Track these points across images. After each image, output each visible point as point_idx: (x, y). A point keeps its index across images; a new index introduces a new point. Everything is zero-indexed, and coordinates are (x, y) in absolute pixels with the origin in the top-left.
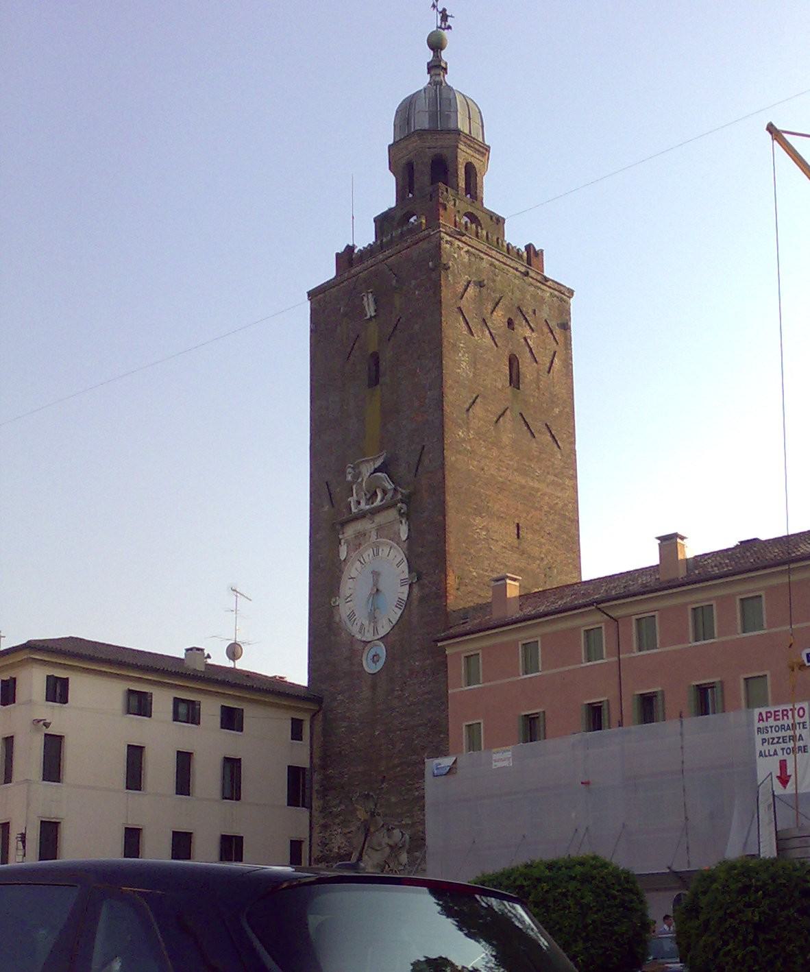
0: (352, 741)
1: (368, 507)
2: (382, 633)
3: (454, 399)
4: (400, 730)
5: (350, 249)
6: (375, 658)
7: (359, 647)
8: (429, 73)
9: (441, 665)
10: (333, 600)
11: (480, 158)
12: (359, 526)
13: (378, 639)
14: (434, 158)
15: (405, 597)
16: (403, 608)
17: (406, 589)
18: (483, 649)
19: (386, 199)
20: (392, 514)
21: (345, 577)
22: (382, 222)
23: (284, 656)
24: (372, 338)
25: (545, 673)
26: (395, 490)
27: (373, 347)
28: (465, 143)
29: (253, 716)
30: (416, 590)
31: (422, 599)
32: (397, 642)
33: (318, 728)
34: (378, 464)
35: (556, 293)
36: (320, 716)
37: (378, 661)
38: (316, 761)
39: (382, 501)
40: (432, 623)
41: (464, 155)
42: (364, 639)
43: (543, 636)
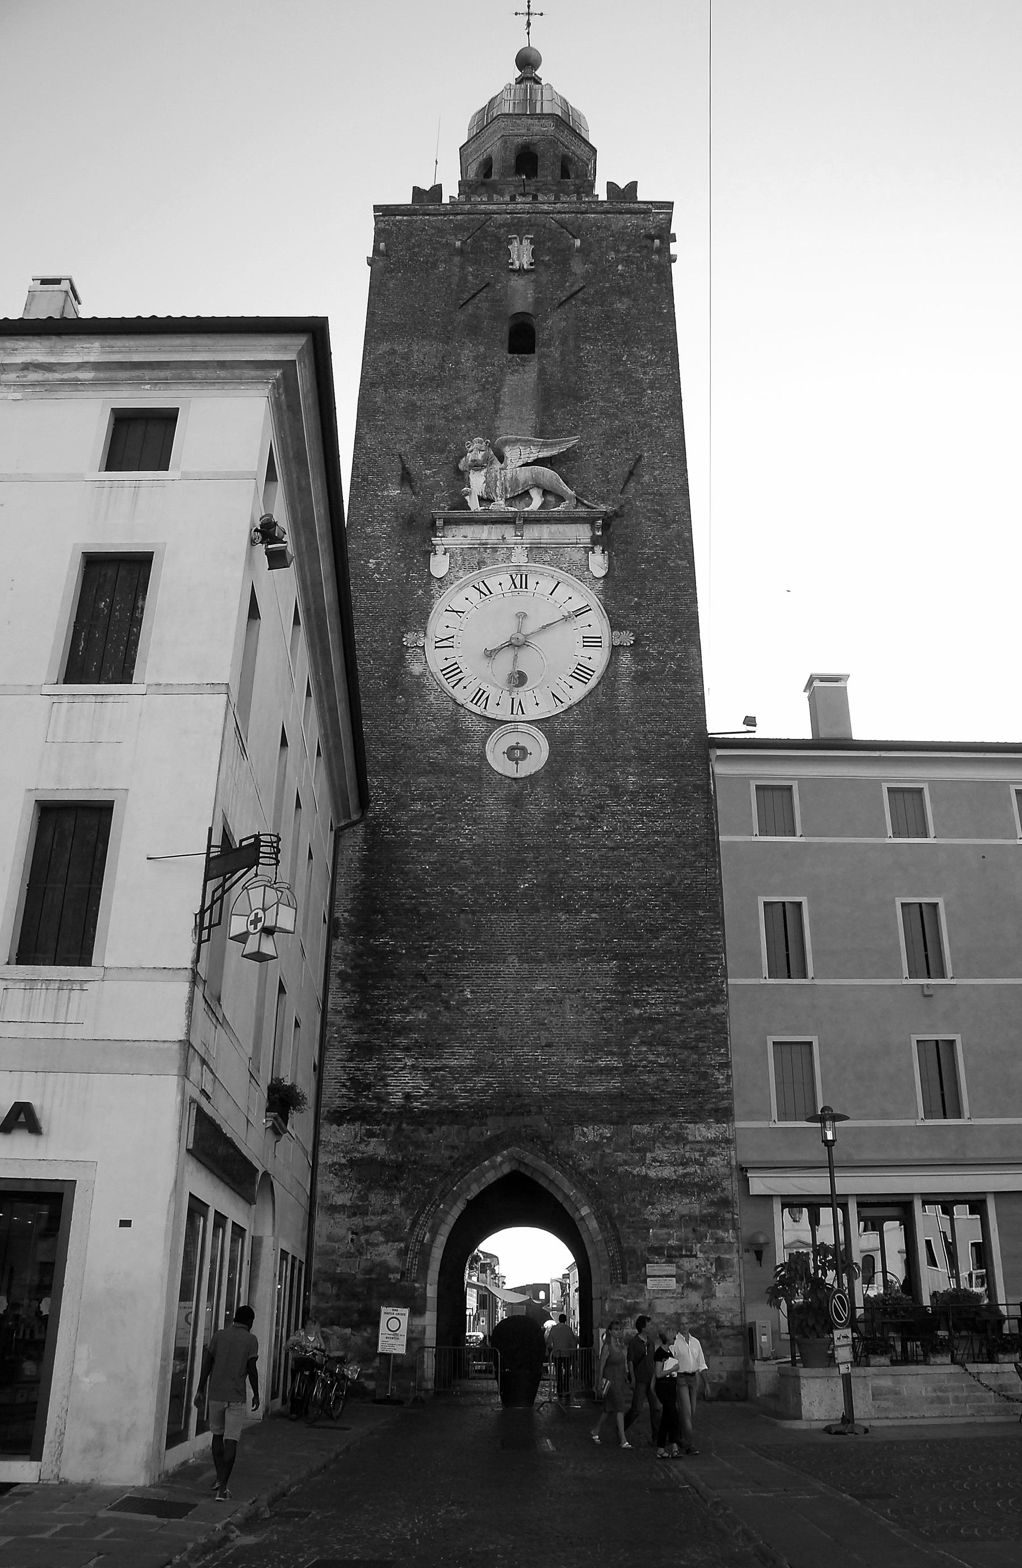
0: (452, 892)
4: (591, 889)
18: (801, 781)
20: (583, 533)
21: (439, 605)
24: (522, 296)
31: (641, 678)
34: (545, 453)
36: (360, 829)
37: (524, 758)
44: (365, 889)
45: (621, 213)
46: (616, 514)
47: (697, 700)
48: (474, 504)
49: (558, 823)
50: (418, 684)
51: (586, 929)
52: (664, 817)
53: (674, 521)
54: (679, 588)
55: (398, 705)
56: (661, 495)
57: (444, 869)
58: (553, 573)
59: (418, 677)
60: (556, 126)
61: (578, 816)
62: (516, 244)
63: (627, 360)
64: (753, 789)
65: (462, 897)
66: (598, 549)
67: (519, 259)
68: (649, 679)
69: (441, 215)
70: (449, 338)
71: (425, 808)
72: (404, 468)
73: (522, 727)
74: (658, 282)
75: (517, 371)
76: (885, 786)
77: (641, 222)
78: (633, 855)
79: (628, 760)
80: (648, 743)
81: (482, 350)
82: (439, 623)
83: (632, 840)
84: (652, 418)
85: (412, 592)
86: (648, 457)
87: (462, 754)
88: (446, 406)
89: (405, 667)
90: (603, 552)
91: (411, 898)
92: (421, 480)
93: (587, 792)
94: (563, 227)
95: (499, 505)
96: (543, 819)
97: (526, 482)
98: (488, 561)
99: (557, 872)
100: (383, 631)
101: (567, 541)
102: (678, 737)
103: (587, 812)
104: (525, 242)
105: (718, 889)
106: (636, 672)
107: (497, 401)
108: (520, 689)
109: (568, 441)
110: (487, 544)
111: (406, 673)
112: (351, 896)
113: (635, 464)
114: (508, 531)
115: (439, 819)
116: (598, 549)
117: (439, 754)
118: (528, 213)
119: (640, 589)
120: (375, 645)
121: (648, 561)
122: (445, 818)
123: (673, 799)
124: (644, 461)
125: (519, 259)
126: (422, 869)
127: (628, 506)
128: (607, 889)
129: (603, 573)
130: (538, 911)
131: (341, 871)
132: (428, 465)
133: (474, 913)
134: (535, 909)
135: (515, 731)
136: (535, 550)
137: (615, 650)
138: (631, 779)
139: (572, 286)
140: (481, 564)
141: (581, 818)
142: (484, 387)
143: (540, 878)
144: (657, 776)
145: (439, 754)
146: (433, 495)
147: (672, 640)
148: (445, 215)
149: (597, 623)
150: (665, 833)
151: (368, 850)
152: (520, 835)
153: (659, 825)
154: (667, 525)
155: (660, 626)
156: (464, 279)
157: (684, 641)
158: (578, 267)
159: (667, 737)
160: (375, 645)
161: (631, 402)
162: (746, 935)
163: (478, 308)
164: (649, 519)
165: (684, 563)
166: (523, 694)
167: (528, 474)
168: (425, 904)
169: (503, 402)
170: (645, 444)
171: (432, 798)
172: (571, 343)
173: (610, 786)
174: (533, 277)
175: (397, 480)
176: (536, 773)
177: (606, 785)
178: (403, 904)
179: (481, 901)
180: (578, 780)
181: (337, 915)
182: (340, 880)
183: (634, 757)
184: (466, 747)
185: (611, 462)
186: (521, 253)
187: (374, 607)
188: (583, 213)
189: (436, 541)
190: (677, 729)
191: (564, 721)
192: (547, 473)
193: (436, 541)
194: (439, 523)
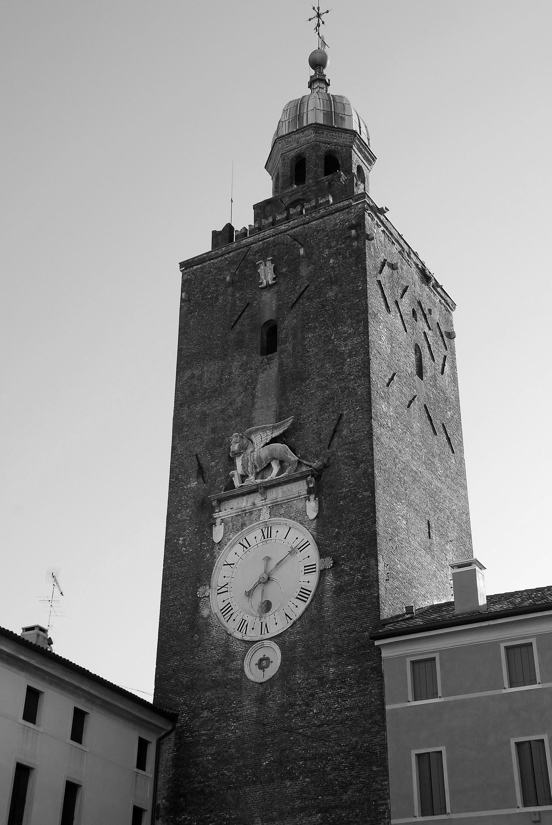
0: (223, 774)
1: (259, 481)
2: (274, 631)
3: (379, 370)
4: (305, 759)
5: (229, 228)
6: (264, 663)
7: (238, 648)
8: (310, 87)
9: (373, 672)
10: (201, 590)
11: (367, 165)
12: (244, 503)
13: (270, 639)
14: (319, 162)
15: (312, 587)
16: (309, 601)
17: (314, 578)
18: (441, 652)
19: (265, 190)
20: (301, 487)
21: (219, 562)
22: (261, 209)
23: (127, 656)
24: (268, 305)
25: (546, 685)
26: (299, 463)
27: (268, 315)
28: (358, 146)
29: (98, 723)
30: (329, 578)
31: (339, 590)
32: (301, 643)
33: (168, 754)
34: (276, 434)
35: (443, 301)
36: (172, 736)
37: (267, 666)
38: (161, 802)
39: (278, 474)
40: (351, 621)
41: (357, 159)
42: (246, 638)
43: (540, 637)
44: (174, 780)
45: (332, 214)
46: (325, 466)
47: (374, 600)
48: (237, 483)
49: (286, 712)
50: (206, 623)
51: (302, 791)
52: (351, 697)
53: (362, 462)
54: (364, 515)
55: (195, 641)
56: (354, 442)
57: (219, 758)
58: (285, 522)
59: (206, 619)
60: (316, 132)
61: (299, 704)
62: (262, 267)
63: (335, 338)
64: (408, 665)
65: (229, 777)
66: (312, 497)
67: (265, 278)
68: (344, 590)
69: (220, 256)
70: (225, 355)
71: (210, 714)
72: (199, 465)
73: (267, 643)
74: (356, 266)
75: (265, 369)
76: (502, 646)
77: (346, 217)
78: (331, 729)
79: (329, 656)
80: (342, 641)
81: (245, 358)
82: (220, 575)
83: (331, 717)
84: (349, 382)
85: (203, 556)
86: (347, 414)
87: (231, 670)
88: (223, 410)
89: (200, 612)
90: (315, 499)
91: (200, 782)
92: (208, 470)
93: (304, 686)
94: (295, 240)
95: (252, 480)
96: (277, 710)
97: (266, 458)
98: (247, 523)
99: (285, 750)
100: (186, 589)
101: (293, 496)
102: (362, 632)
103: (304, 700)
104: (268, 264)
105: (384, 747)
106: (335, 587)
107: (254, 396)
108: (268, 614)
109: (287, 421)
110: (246, 510)
111: (199, 617)
112: (167, 787)
113: (338, 422)
114: (257, 499)
115: (217, 721)
116: (312, 497)
117: (217, 673)
118: (273, 236)
119: (339, 521)
120: (182, 600)
121: (344, 498)
122: (221, 720)
123: (358, 681)
124: (344, 417)
125: (265, 278)
126: (208, 760)
127: (333, 458)
128: (316, 758)
129: (315, 514)
130: (273, 781)
131: (161, 769)
132: (213, 458)
133: (236, 788)
134: (271, 780)
135: (263, 647)
136: (275, 508)
137: (323, 573)
138: (332, 670)
139: (300, 288)
140: (243, 525)
141: (300, 706)
142: (246, 388)
143: (275, 756)
144: (348, 665)
145: (218, 673)
146: (215, 480)
147: (359, 556)
148: (222, 255)
149: (312, 553)
150: (351, 709)
151: (177, 751)
152: (264, 725)
153: (349, 703)
154: (357, 466)
155: (351, 547)
156: (234, 304)
157: (367, 556)
158: (304, 271)
159: (354, 633)
160: (182, 600)
161: (336, 373)
162: (404, 780)
163: (243, 325)
164: (346, 464)
165: (368, 493)
166: (269, 618)
167: (267, 452)
168: (209, 786)
169: (258, 397)
170: (345, 404)
171: (214, 706)
172: (299, 335)
173: (318, 678)
174: (276, 289)
175: (195, 475)
176: (273, 676)
177: (316, 678)
178: (196, 788)
179: (240, 779)
180: (299, 677)
181: (159, 802)
182: (161, 776)
183: (333, 653)
184: (232, 665)
185: (323, 426)
186: (266, 274)
187: (182, 573)
188: (307, 223)
189: (216, 515)
190: (361, 626)
191: (291, 634)
192: (278, 446)
193: (216, 515)
194: (214, 503)
